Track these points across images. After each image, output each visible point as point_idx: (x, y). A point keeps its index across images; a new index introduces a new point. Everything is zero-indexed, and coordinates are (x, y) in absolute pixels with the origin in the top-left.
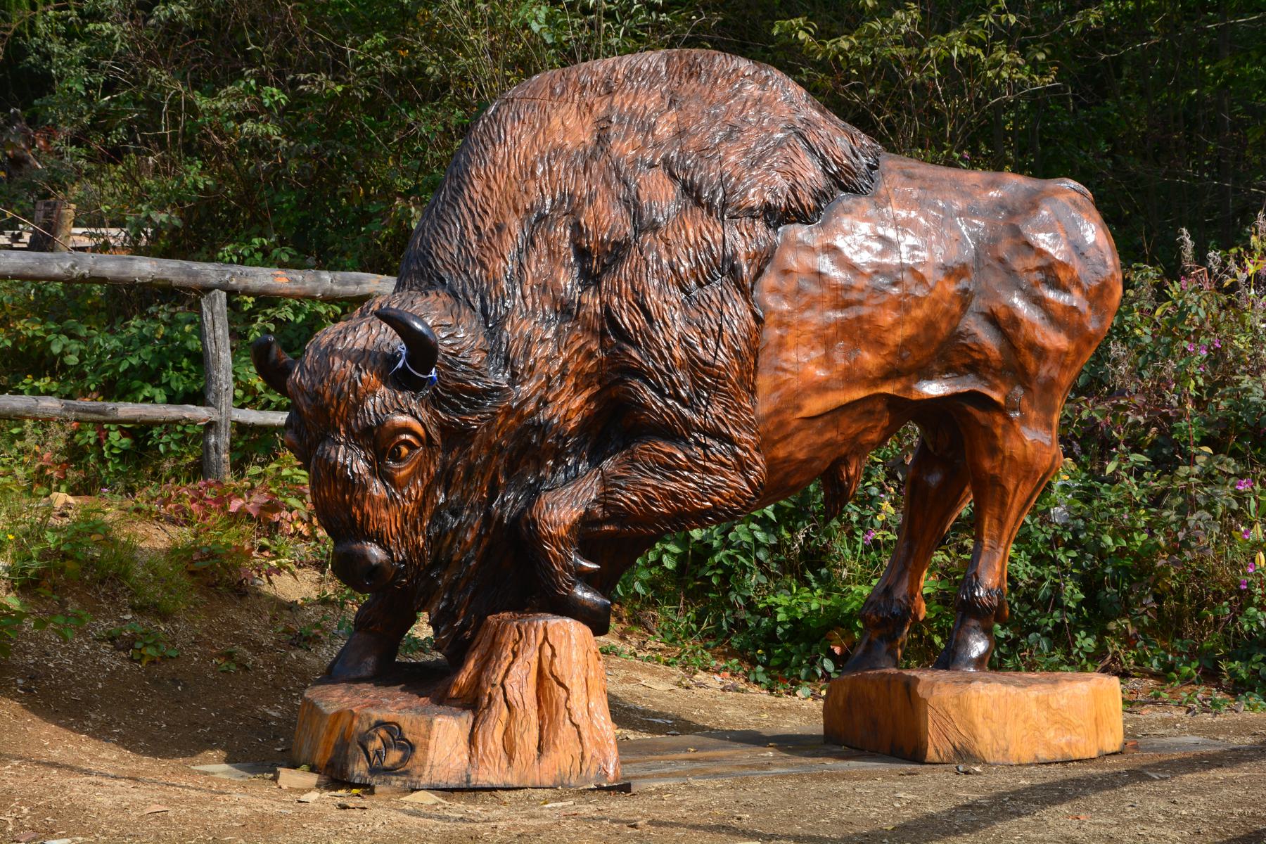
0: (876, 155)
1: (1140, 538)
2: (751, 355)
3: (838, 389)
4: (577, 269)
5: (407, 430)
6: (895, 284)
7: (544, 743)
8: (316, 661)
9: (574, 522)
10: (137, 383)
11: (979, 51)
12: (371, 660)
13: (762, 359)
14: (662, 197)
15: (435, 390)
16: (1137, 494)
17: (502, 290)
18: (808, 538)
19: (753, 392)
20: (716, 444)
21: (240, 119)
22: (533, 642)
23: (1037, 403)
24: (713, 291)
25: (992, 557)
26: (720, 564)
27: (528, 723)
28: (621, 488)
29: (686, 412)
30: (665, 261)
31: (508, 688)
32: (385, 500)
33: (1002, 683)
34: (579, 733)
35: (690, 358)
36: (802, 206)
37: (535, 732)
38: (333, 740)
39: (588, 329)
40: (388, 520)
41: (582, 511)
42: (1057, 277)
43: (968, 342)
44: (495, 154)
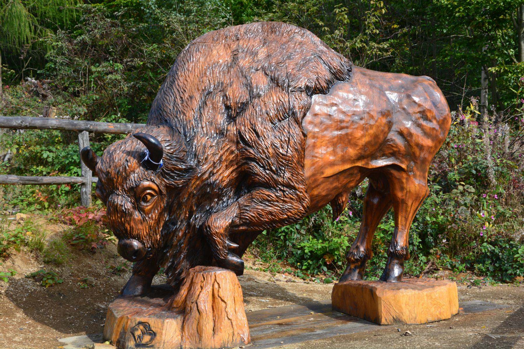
0: (350, 66)
1: (441, 218)
2: (301, 151)
3: (339, 165)
4: (226, 115)
5: (150, 188)
6: (361, 119)
7: (216, 328)
8: (123, 280)
9: (227, 226)
10: (72, 167)
11: (365, 45)
12: (140, 287)
13: (306, 152)
14: (262, 83)
15: (163, 170)
16: (438, 201)
17: (192, 125)
18: (315, 220)
19: (303, 167)
20: (288, 190)
21: (107, 74)
22: (210, 282)
23: (419, 169)
24: (285, 123)
25: (402, 232)
26: (284, 231)
27: (208, 319)
28: (247, 210)
29: (275, 176)
30: (264, 111)
31: (199, 304)
32: (141, 220)
33: (412, 289)
34: (232, 323)
35: (276, 153)
36: (322, 87)
37: (212, 324)
38: (120, 330)
39: (231, 141)
40: (143, 230)
41: (230, 221)
42: (427, 116)
43: (391, 143)
44: (189, 66)
